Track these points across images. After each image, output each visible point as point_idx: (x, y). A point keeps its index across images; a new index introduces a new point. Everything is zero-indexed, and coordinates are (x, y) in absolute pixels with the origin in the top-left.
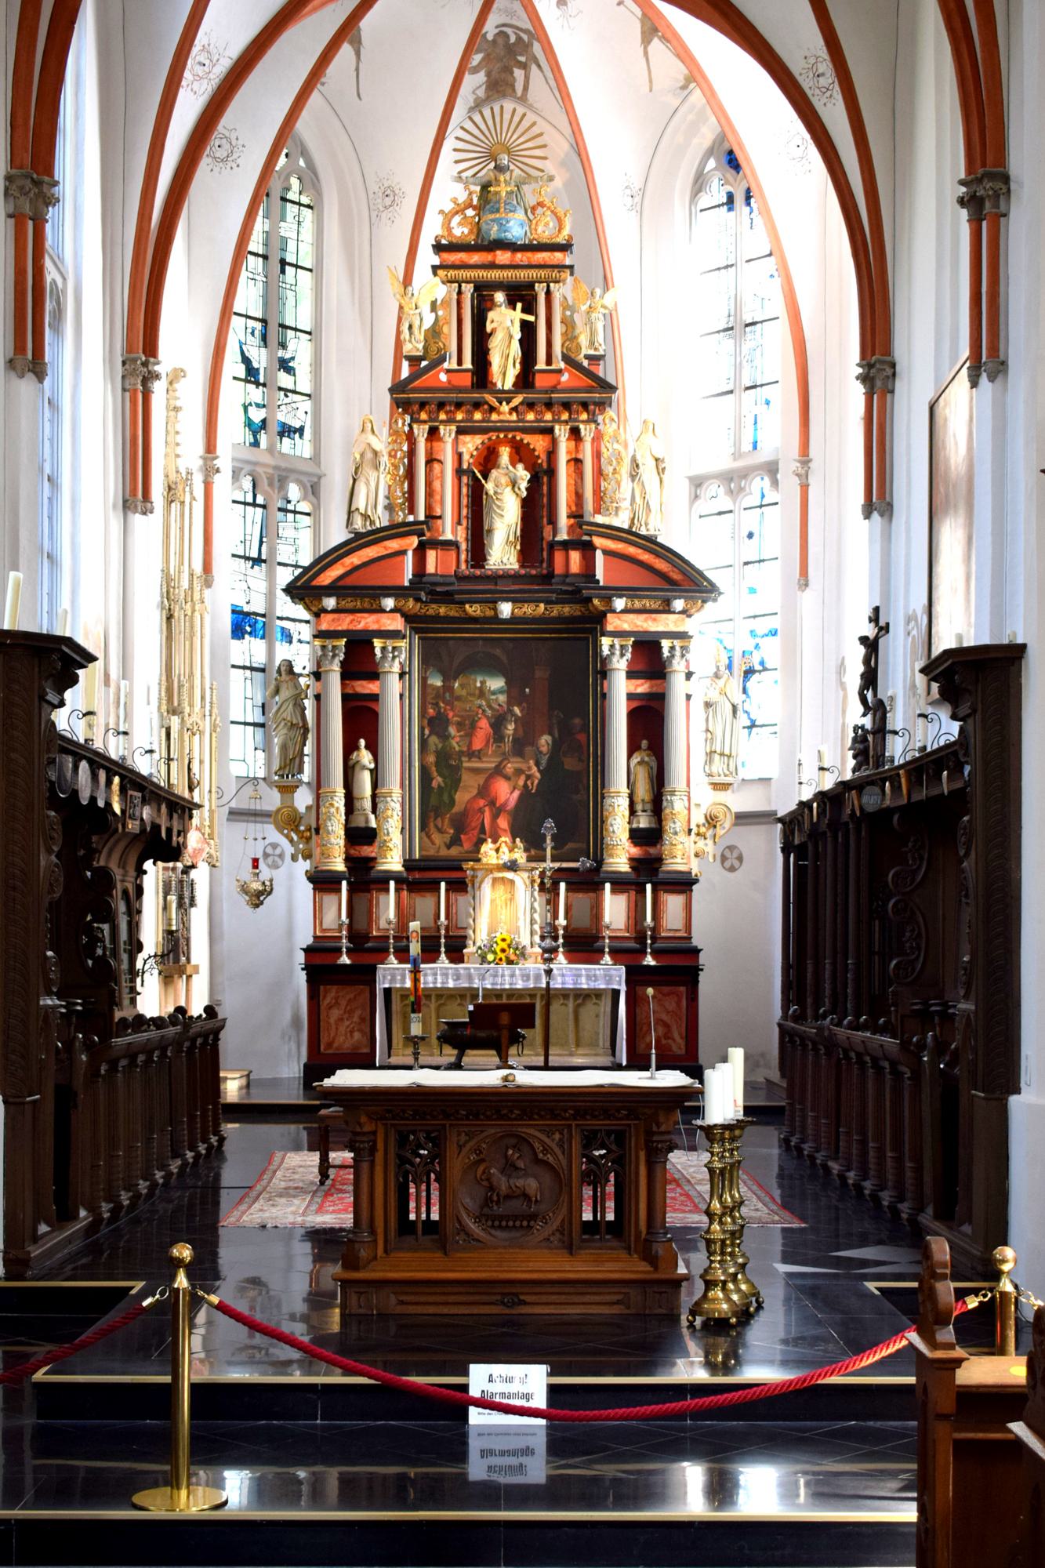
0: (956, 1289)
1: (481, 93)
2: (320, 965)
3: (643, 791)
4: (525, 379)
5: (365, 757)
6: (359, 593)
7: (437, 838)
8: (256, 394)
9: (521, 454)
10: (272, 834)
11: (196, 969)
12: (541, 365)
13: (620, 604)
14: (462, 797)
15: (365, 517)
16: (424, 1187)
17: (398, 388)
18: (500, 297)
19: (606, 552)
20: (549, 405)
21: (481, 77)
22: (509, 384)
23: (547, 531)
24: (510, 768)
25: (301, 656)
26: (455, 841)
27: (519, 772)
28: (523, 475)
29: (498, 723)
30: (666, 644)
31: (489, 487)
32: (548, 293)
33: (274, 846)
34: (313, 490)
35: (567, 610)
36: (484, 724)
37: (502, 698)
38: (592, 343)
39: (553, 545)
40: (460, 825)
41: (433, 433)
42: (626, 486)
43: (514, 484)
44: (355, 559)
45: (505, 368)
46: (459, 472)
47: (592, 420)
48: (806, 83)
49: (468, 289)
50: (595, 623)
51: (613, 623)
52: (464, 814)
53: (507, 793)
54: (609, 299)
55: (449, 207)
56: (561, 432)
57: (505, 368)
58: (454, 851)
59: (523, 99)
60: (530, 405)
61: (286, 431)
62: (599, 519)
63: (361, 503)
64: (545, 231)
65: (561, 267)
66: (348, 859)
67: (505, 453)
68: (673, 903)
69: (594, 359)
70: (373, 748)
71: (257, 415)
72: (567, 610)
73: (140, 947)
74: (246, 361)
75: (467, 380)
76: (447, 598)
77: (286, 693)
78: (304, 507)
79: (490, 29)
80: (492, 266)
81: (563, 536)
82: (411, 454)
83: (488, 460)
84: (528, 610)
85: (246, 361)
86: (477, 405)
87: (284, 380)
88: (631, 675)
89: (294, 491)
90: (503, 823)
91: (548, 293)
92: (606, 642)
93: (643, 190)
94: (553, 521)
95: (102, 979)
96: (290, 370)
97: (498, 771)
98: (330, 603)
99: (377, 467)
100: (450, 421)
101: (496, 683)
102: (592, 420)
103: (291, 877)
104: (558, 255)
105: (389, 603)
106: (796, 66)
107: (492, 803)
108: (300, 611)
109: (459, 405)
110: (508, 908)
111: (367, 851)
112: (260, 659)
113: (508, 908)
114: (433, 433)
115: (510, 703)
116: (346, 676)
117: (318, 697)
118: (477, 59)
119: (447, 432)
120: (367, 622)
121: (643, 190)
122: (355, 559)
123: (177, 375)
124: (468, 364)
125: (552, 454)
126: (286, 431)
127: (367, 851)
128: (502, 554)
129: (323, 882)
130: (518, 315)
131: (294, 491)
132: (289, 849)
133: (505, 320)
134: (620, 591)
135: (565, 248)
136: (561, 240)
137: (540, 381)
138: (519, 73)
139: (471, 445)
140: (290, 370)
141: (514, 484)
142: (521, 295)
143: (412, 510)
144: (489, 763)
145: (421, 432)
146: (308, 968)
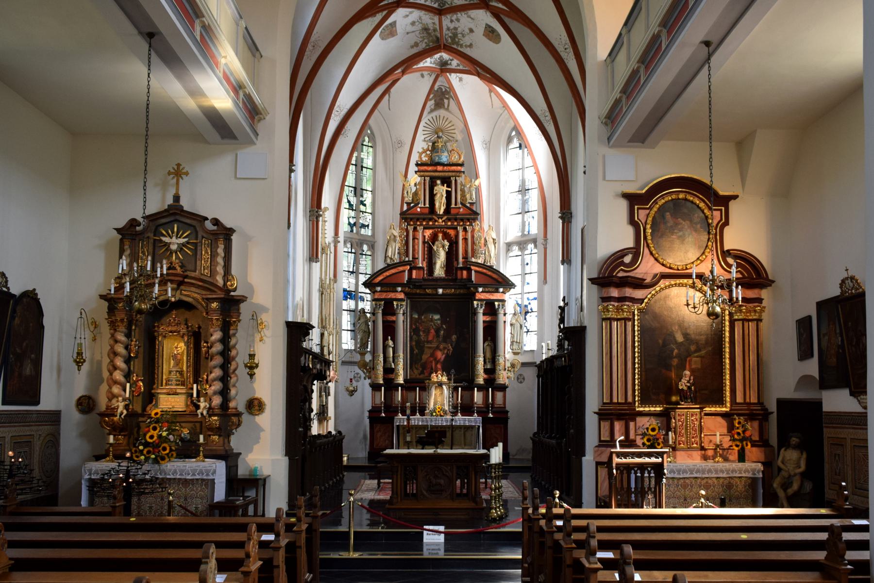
1: (433, 107)
2: (374, 413)
3: (488, 355)
6: (389, 285)
7: (416, 372)
8: (353, 214)
9: (446, 236)
11: (330, 418)
12: (453, 206)
13: (480, 290)
14: (425, 357)
15: (391, 259)
16: (220, 250)
17: (403, 214)
18: (439, 182)
19: (476, 271)
20: (456, 220)
21: (433, 102)
22: (442, 212)
23: (455, 263)
24: (441, 347)
25: (367, 306)
26: (422, 373)
27: (445, 348)
28: (447, 243)
29: (437, 331)
30: (496, 303)
31: (435, 248)
32: (456, 180)
33: (358, 374)
34: (372, 247)
36: (432, 331)
37: (439, 322)
38: (471, 198)
39: (457, 269)
40: (424, 366)
41: (415, 229)
44: (387, 274)
46: (424, 242)
47: (471, 225)
48: (542, 119)
49: (428, 179)
50: (472, 296)
51: (478, 296)
52: (425, 363)
53: (440, 355)
54: (477, 183)
55: (421, 150)
56: (460, 229)
58: (422, 376)
59: (447, 109)
60: (449, 220)
61: (364, 226)
62: (473, 260)
64: (455, 158)
65: (460, 172)
66: (384, 379)
67: (440, 236)
68: (499, 395)
71: (352, 221)
73: (312, 411)
74: (349, 202)
75: (427, 211)
76: (420, 287)
77: (362, 320)
78: (369, 253)
79: (436, 88)
80: (436, 171)
81: (461, 265)
83: (434, 238)
84: (448, 291)
85: (349, 202)
86: (430, 219)
87: (362, 208)
88: (484, 314)
89: (365, 247)
90: (439, 366)
91: (456, 180)
92: (475, 303)
93: (490, 142)
94: (457, 260)
96: (365, 205)
97: (438, 348)
98: (379, 289)
101: (437, 317)
102: (471, 225)
103: (363, 385)
104: (459, 168)
105: (399, 289)
107: (435, 359)
108: (368, 291)
109: (424, 220)
112: (353, 307)
113: (440, 398)
114: (415, 229)
115: (442, 324)
117: (374, 322)
118: (432, 96)
120: (392, 295)
121: (490, 142)
122: (387, 274)
123: (326, 209)
124: (427, 205)
125: (457, 236)
126: (364, 226)
128: (439, 271)
129: (375, 387)
130: (445, 188)
131: (365, 247)
132: (363, 375)
133: (441, 190)
134: (480, 286)
135: (462, 165)
136: (460, 162)
137: (452, 211)
138: (446, 101)
139: (428, 233)
140: (365, 205)
141: (443, 247)
142: (446, 181)
143: (407, 256)
144: (434, 345)
145: (411, 229)
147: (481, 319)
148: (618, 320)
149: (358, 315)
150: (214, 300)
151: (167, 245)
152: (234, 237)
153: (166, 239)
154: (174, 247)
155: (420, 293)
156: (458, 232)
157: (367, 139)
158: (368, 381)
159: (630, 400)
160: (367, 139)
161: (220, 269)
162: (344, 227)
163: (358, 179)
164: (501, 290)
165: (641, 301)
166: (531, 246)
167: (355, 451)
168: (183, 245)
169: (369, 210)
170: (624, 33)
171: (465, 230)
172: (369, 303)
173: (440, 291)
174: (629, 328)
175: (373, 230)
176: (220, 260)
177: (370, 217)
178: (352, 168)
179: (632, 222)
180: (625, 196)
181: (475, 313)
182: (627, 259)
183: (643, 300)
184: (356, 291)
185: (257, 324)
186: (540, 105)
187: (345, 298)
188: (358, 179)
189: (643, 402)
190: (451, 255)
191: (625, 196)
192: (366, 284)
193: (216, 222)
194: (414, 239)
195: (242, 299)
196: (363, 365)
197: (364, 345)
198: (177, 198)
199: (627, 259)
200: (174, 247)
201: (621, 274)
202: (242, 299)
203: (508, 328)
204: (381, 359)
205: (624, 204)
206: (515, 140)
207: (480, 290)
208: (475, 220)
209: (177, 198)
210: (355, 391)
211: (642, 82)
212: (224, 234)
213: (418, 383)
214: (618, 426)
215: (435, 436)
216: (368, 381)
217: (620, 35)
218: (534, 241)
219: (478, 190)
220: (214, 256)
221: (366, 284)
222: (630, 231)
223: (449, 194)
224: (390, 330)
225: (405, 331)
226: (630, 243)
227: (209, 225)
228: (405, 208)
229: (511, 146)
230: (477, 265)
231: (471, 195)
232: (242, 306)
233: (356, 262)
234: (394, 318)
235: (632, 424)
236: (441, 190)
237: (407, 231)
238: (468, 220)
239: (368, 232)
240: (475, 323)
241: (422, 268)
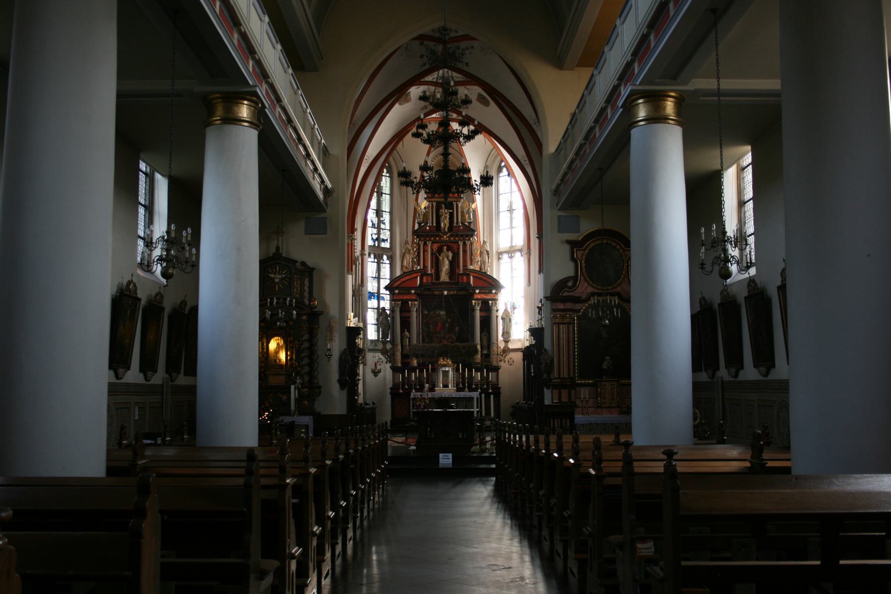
0: (185, 374)
2: (394, 390)
3: (485, 342)
4: (451, 227)
5: (407, 333)
6: (405, 290)
8: (375, 231)
10: (379, 355)
16: (307, 283)
17: (415, 233)
20: (457, 236)
25: (386, 304)
28: (450, 254)
31: (441, 258)
34: (391, 259)
35: (463, 293)
38: (469, 218)
39: (459, 274)
41: (425, 244)
42: (479, 258)
43: (448, 257)
44: (403, 280)
45: (445, 223)
46: (432, 254)
48: (522, 162)
49: (434, 204)
50: (471, 295)
51: (476, 296)
54: (473, 206)
56: (461, 243)
57: (445, 223)
60: (451, 236)
61: (384, 240)
62: (472, 267)
63: (405, 264)
66: (402, 363)
69: (470, 223)
70: (409, 331)
72: (463, 293)
76: (429, 290)
77: (384, 315)
81: (461, 272)
82: (419, 249)
83: (440, 250)
84: (452, 293)
86: (437, 236)
88: (481, 310)
94: (459, 267)
95: (282, 366)
98: (397, 291)
99: (409, 253)
100: (430, 240)
101: (442, 313)
103: (385, 368)
105: (413, 292)
106: (520, 157)
108: (388, 292)
109: (432, 236)
110: (448, 371)
111: (407, 360)
113: (448, 371)
114: (425, 244)
116: (401, 312)
119: (429, 244)
122: (403, 280)
125: (458, 249)
126: (384, 240)
127: (407, 360)
128: (444, 277)
129: (394, 369)
132: (385, 360)
133: (445, 213)
139: (436, 246)
140: (384, 224)
141: (448, 257)
143: (419, 264)
145: (422, 244)
146: (391, 393)
147: (478, 314)
148: (563, 324)
149: (381, 312)
150: (304, 314)
151: (273, 279)
152: (314, 273)
153: (272, 276)
154: (277, 280)
155: (428, 294)
156: (459, 245)
157: (385, 170)
158: (389, 365)
159: (572, 375)
160: (385, 170)
161: (306, 294)
162: (369, 242)
163: (379, 203)
164: (494, 291)
165: (579, 311)
166: (518, 254)
167: (386, 416)
168: (283, 279)
169: (388, 227)
170: (586, 93)
171: (465, 244)
172: (388, 302)
173: (446, 293)
174: (571, 329)
175: (391, 243)
176: (306, 288)
177: (388, 233)
178: (375, 194)
179: (573, 259)
180: (569, 242)
181: (473, 310)
182: (570, 284)
183: (579, 311)
184: (378, 293)
185: (330, 329)
186: (521, 153)
187: (370, 298)
188: (379, 203)
189: (581, 378)
190: (454, 264)
191: (569, 242)
192: (386, 288)
193: (303, 264)
194: (424, 251)
195: (322, 313)
196: (384, 352)
197: (385, 336)
198: (278, 248)
199: (570, 284)
200: (277, 280)
201: (565, 294)
202: (322, 313)
203: (500, 322)
204: (400, 348)
205: (567, 247)
206: (505, 170)
207: (477, 291)
208: (472, 236)
209: (278, 248)
210: (379, 371)
211: (652, 46)
212: (308, 271)
213: (429, 363)
214: (564, 393)
215: (444, 402)
216: (389, 365)
217: (567, 129)
218: (520, 251)
219: (475, 212)
220: (302, 285)
221: (386, 288)
222: (571, 265)
223: (451, 215)
224: (406, 324)
225: (418, 324)
226: (571, 273)
227: (298, 265)
228: (416, 227)
229: (501, 175)
230: (474, 271)
231: (469, 216)
232: (320, 317)
233: (379, 270)
234: (323, 215)
235: (573, 392)
236: (445, 213)
237: (419, 245)
238: (467, 236)
239: (386, 245)
240: (473, 317)
241: (431, 275)
